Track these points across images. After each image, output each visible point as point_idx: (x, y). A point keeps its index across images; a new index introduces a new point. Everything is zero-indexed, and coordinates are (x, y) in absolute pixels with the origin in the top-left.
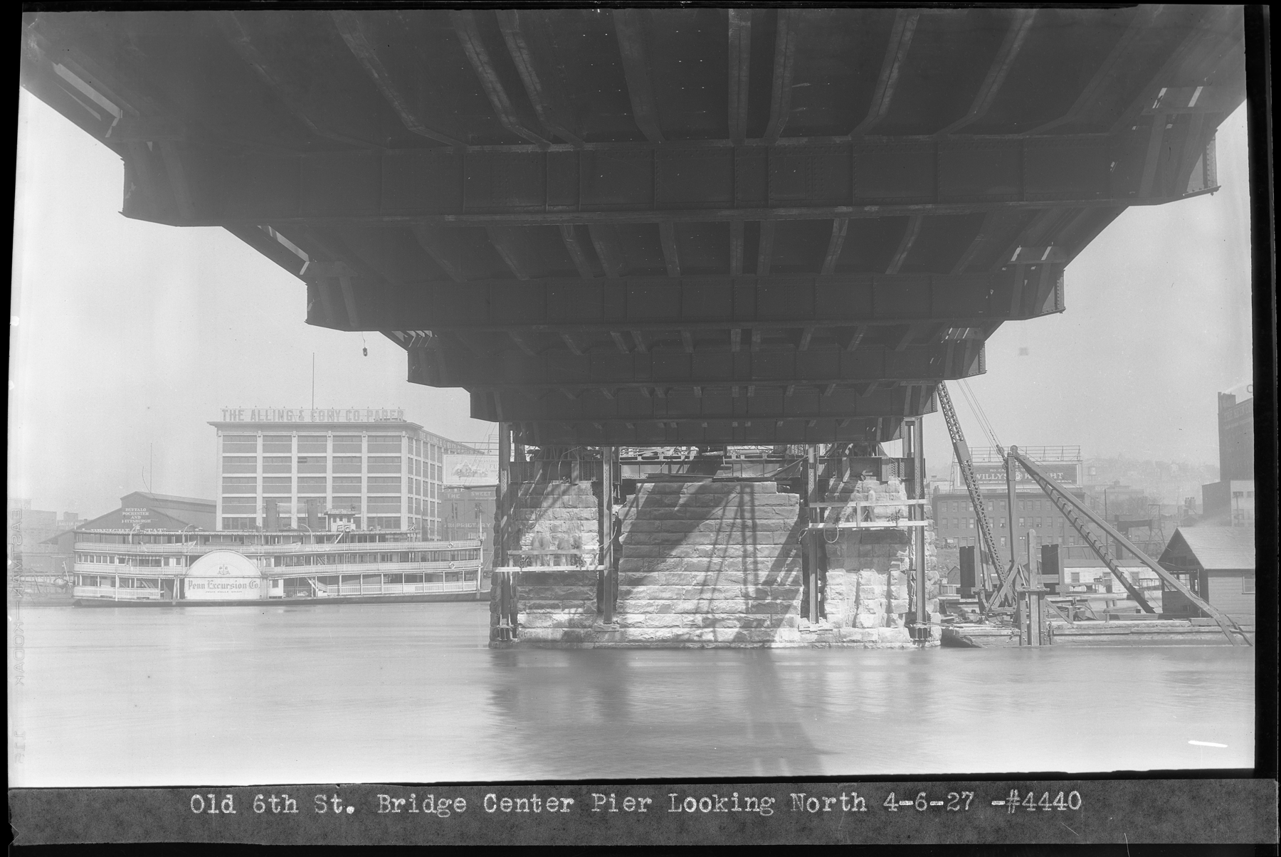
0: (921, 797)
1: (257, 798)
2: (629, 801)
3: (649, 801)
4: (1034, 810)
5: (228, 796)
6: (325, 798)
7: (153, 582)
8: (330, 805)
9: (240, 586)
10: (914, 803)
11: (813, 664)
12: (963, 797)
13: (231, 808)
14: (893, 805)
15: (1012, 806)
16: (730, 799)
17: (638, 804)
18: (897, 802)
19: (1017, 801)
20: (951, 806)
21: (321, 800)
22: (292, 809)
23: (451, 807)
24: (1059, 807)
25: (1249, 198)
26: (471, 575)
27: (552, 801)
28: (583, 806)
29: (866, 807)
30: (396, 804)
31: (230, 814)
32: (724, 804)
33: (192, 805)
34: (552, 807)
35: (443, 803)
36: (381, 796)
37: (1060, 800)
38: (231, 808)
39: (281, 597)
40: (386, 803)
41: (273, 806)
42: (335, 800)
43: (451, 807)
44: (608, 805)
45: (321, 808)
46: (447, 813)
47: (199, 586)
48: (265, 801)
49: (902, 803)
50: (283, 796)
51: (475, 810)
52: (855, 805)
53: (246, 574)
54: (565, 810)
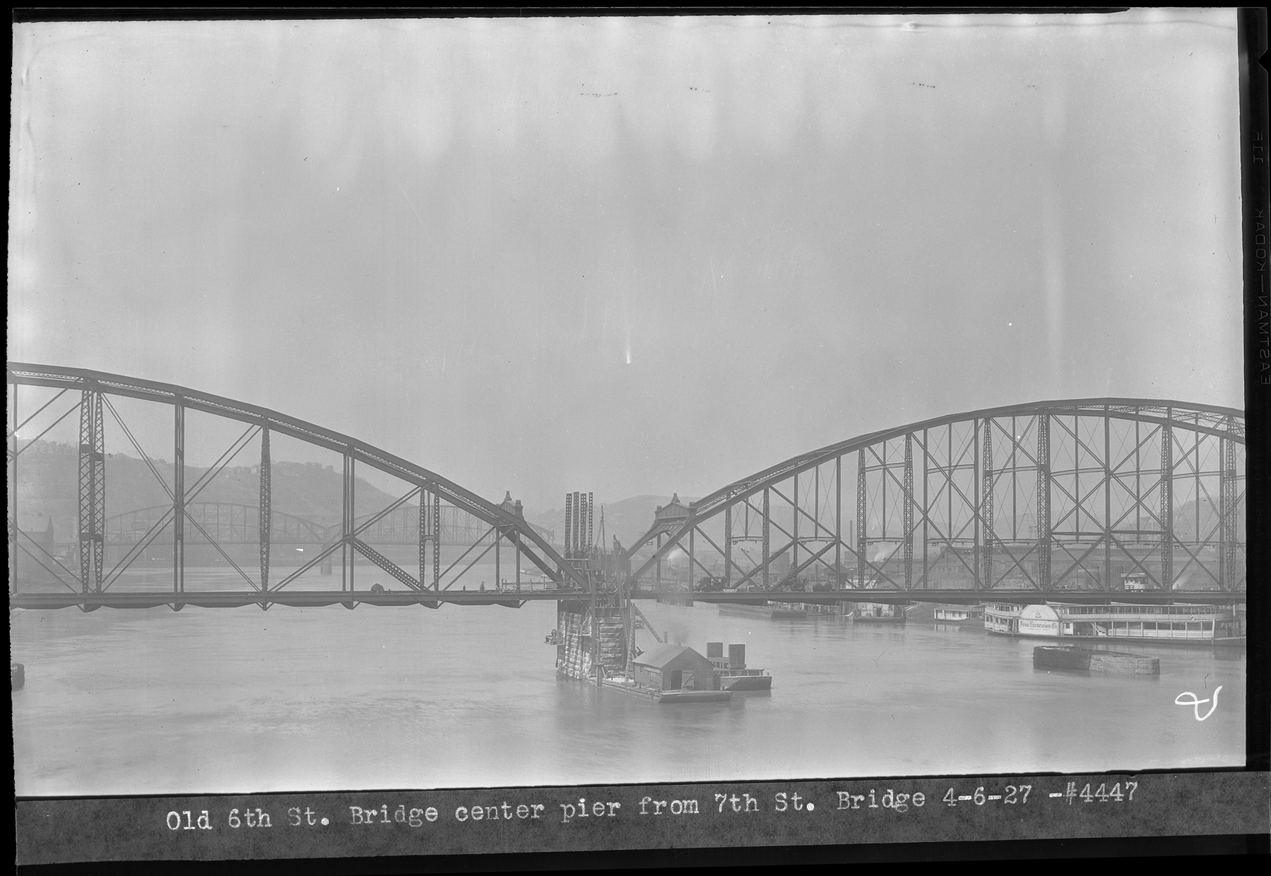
1: (232, 812)
2: (598, 806)
7: (1003, 621)
8: (304, 817)
9: (1047, 626)
12: (1021, 790)
16: (379, 812)
18: (956, 796)
19: (1074, 793)
20: (1008, 799)
21: (781, 798)
22: (753, 808)
24: (1086, 798)
26: (1207, 626)
27: (918, 797)
28: (708, 806)
39: (1071, 635)
40: (358, 815)
43: (422, 817)
45: (781, 806)
47: (1027, 625)
49: (961, 798)
51: (341, 826)
53: (1050, 618)
54: (612, 814)
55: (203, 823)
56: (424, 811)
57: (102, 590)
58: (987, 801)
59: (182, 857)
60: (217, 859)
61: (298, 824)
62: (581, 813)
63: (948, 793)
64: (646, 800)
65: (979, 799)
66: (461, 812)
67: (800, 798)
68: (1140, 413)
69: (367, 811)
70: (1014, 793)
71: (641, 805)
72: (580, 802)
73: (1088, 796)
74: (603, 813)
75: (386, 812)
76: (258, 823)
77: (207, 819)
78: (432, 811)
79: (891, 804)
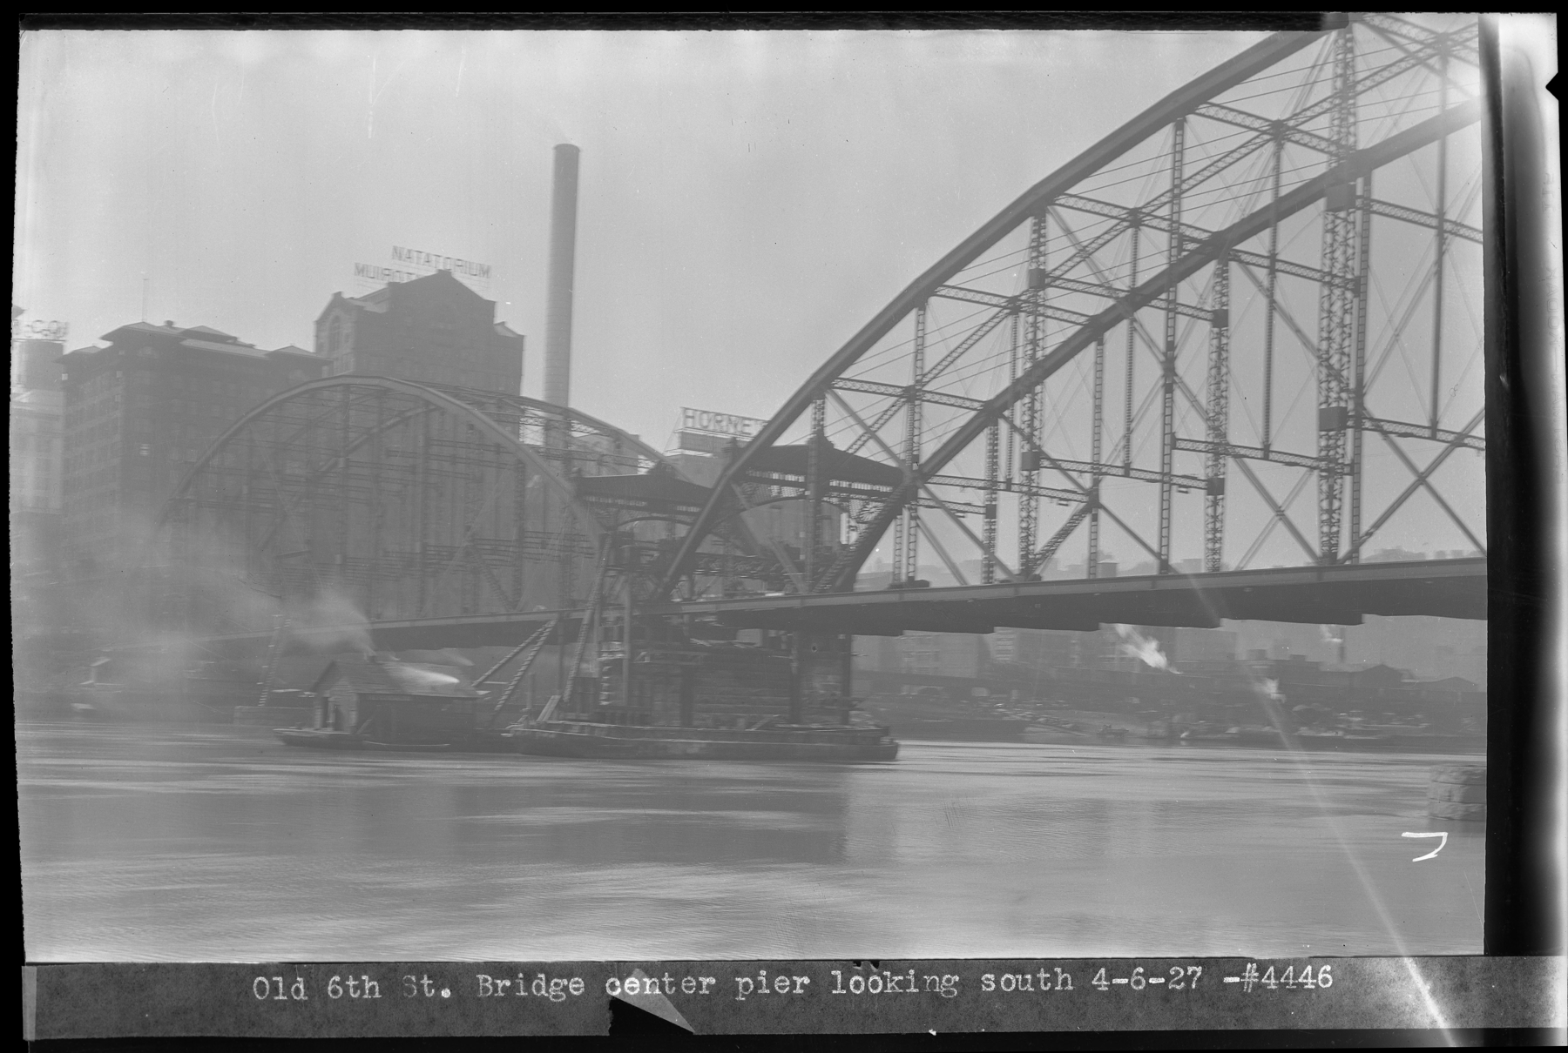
0: (1138, 974)
4: (1107, 989)
6: (413, 978)
8: (420, 987)
11: (187, 878)
13: (302, 994)
14: (1310, 980)
15: (1248, 983)
19: (1255, 977)
20: (1173, 983)
21: (409, 981)
22: (374, 994)
24: (1307, 984)
31: (301, 1000)
32: (898, 983)
33: (255, 989)
34: (689, 988)
35: (948, 981)
36: (481, 977)
37: (1307, 974)
38: (302, 994)
41: (426, 990)
42: (426, 981)
43: (565, 989)
44: (758, 985)
45: (988, 986)
46: (562, 996)
52: (367, 992)
56: (569, 981)
58: (1111, 986)
59: (270, 1033)
61: (1141, 987)
62: (278, 994)
63: (1288, 972)
65: (1138, 983)
67: (431, 982)
69: (499, 981)
73: (1273, 981)
74: (787, 989)
75: (913, 980)
76: (363, 993)
77: (301, 987)
79: (543, 992)
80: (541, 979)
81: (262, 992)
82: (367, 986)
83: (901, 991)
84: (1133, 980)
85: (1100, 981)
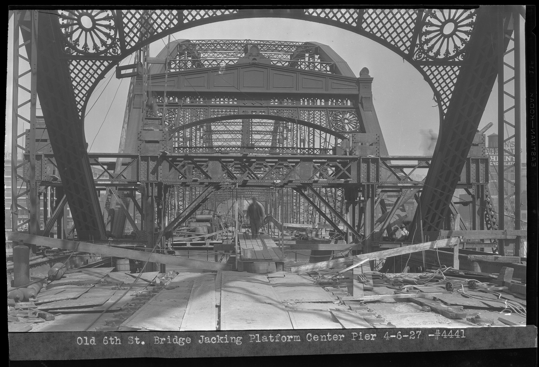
0: (399, 334)
3: (343, 336)
5: (93, 338)
10: (396, 336)
14: (445, 336)
16: (166, 339)
17: (371, 337)
19: (439, 334)
21: (131, 339)
23: (184, 341)
25: (6, 119)
27: (335, 336)
29: (121, 343)
30: (341, 337)
31: (94, 345)
32: (222, 339)
34: (367, 338)
35: (239, 339)
37: (387, 335)
48: (108, 339)
50: (115, 337)
54: (341, 340)
55: (92, 342)
56: (185, 339)
57: (212, 129)
60: (213, 356)
64: (278, 336)
65: (399, 337)
66: (214, 339)
68: (142, 52)
70: (414, 334)
71: (276, 338)
72: (168, 337)
77: (94, 341)
78: (189, 339)
80: (93, 339)
81: (80, 342)
82: (117, 340)
83: (223, 342)
84: (397, 336)
85: (386, 337)
